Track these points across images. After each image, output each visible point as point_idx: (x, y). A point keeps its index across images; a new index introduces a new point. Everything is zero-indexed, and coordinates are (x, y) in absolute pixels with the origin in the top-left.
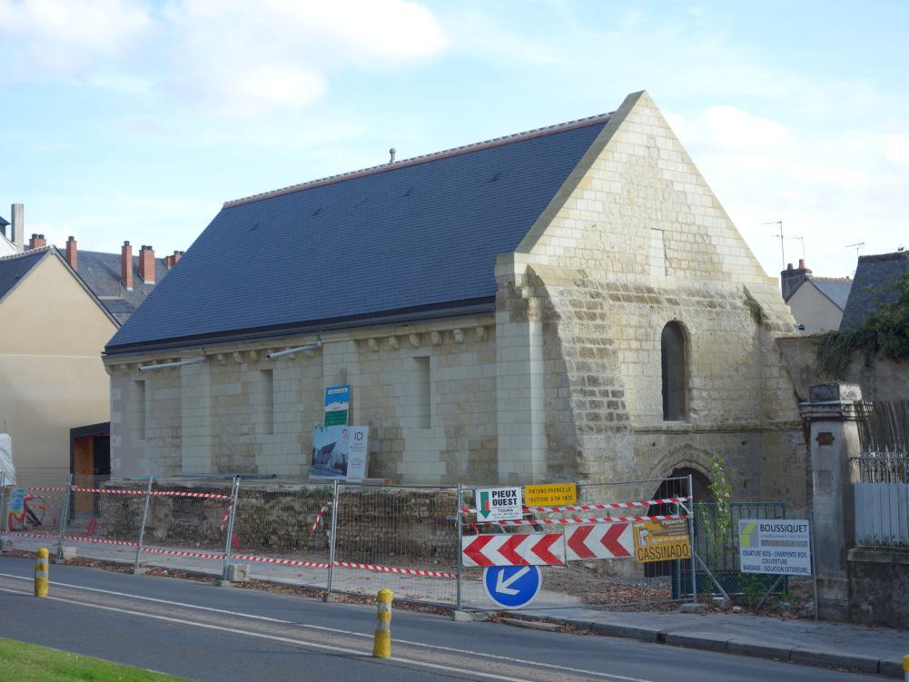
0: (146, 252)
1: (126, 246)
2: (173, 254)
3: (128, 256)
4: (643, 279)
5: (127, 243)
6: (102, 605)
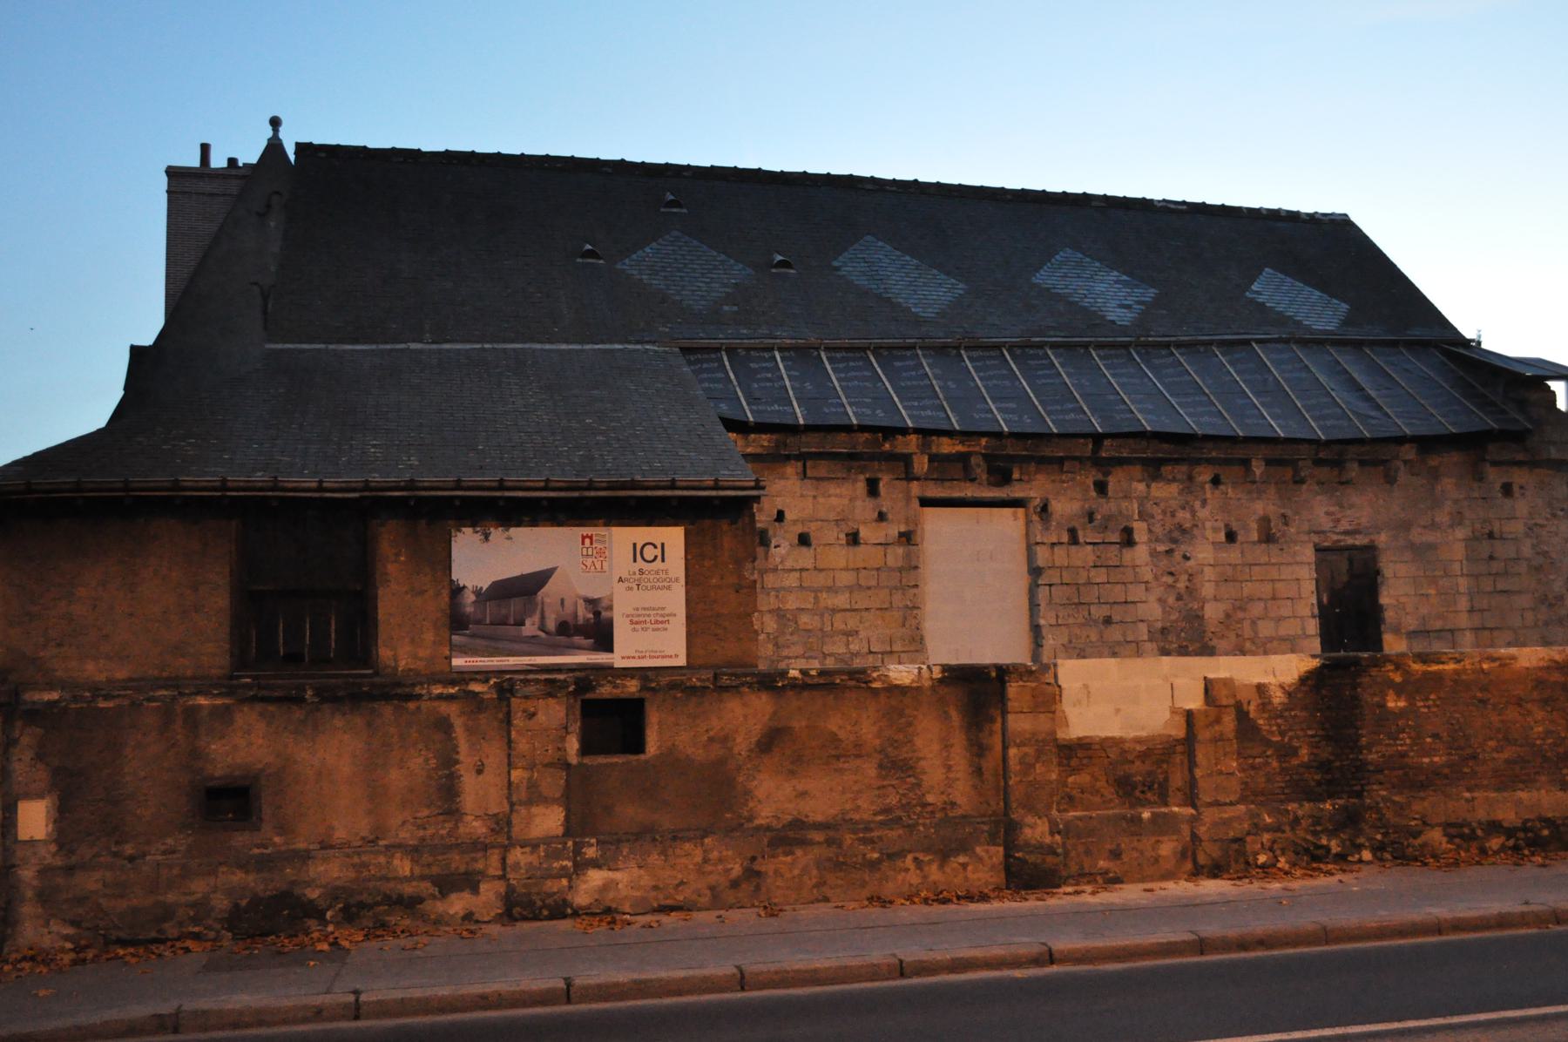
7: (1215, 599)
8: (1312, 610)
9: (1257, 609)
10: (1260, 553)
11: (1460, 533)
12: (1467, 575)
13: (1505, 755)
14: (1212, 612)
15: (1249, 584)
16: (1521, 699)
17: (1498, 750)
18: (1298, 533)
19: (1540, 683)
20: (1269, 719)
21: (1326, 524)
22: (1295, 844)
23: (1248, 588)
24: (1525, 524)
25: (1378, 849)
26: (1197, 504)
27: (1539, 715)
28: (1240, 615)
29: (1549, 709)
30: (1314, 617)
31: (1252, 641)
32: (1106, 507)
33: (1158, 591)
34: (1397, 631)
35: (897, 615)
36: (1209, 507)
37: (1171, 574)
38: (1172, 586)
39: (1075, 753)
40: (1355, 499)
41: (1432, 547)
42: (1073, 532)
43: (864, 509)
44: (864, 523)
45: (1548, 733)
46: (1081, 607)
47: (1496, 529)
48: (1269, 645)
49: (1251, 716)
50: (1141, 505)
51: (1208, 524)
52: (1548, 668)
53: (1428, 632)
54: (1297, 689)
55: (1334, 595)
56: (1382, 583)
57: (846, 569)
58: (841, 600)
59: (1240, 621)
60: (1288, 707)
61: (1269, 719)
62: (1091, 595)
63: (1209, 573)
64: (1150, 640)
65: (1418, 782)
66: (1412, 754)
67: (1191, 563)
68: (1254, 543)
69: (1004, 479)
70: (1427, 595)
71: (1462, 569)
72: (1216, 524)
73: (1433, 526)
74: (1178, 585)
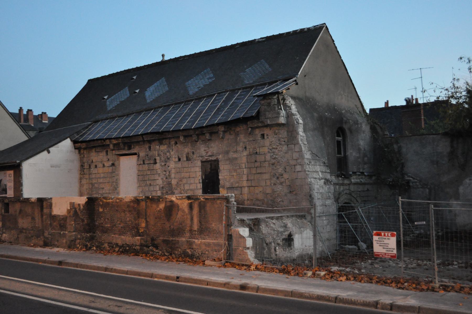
0: (30, 112)
1: (21, 109)
2: (41, 113)
3: (22, 113)
4: (289, 255)
5: (21, 108)
6: (218, 91)
7: (175, 178)
8: (199, 181)
9: (184, 181)
10: (186, 164)
11: (245, 153)
12: (247, 168)
13: (121, 226)
14: (174, 182)
15: (183, 173)
16: (125, 210)
17: (120, 224)
18: (196, 157)
19: (128, 206)
20: (80, 212)
21: (204, 154)
22: (83, 244)
23: (183, 175)
24: (268, 148)
25: (97, 247)
26: (171, 151)
27: (128, 215)
28: (181, 183)
29: (130, 213)
30: (200, 183)
31: (183, 190)
32: (150, 153)
33: (162, 176)
34: (223, 187)
35: (110, 184)
36: (174, 151)
37: (165, 171)
38: (165, 175)
39: (55, 217)
40: (212, 145)
41: (236, 159)
42: (144, 161)
43: (105, 159)
44: (105, 162)
45: (130, 220)
46: (145, 181)
47: (258, 151)
48: (187, 192)
49: (78, 211)
50: (158, 152)
51: (173, 156)
52: (131, 202)
53: (233, 188)
54: (85, 205)
55: (206, 176)
56: (220, 171)
57: (102, 173)
58: (101, 180)
59: (180, 185)
60: (83, 209)
61: (80, 212)
62: (146, 178)
63: (173, 171)
64: (159, 190)
65: (105, 231)
66: (104, 223)
67: (169, 168)
68: (185, 161)
69: (130, 148)
70: (233, 175)
71: (245, 166)
72: (175, 156)
73: (236, 152)
74: (167, 174)
